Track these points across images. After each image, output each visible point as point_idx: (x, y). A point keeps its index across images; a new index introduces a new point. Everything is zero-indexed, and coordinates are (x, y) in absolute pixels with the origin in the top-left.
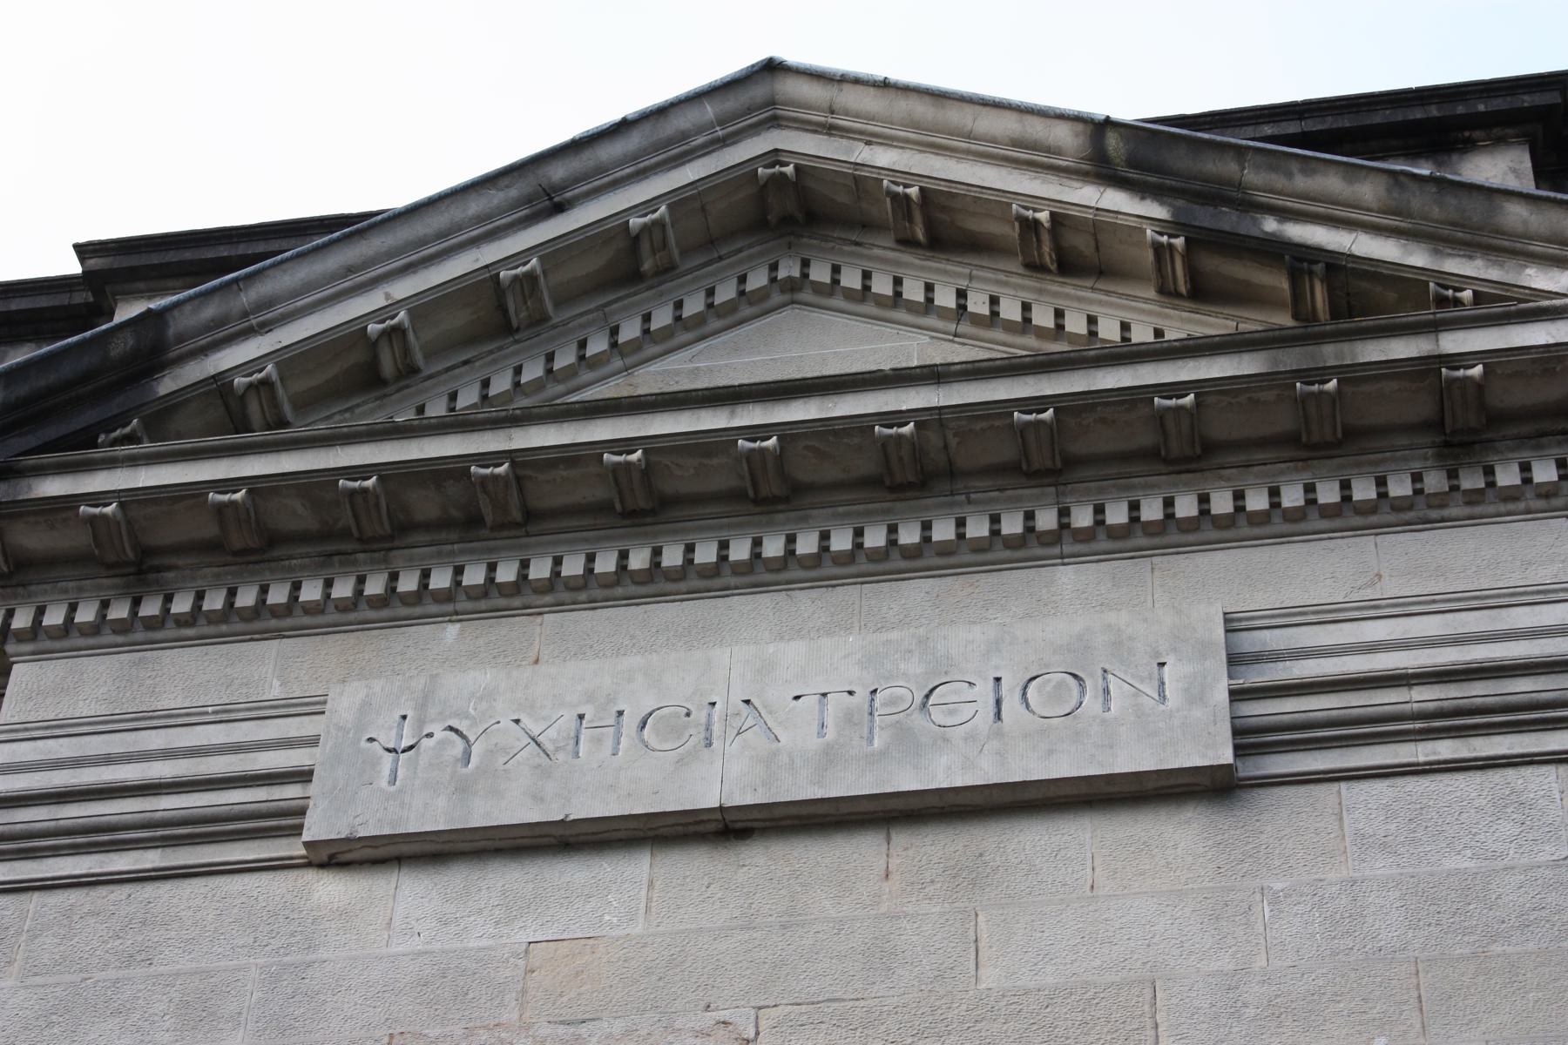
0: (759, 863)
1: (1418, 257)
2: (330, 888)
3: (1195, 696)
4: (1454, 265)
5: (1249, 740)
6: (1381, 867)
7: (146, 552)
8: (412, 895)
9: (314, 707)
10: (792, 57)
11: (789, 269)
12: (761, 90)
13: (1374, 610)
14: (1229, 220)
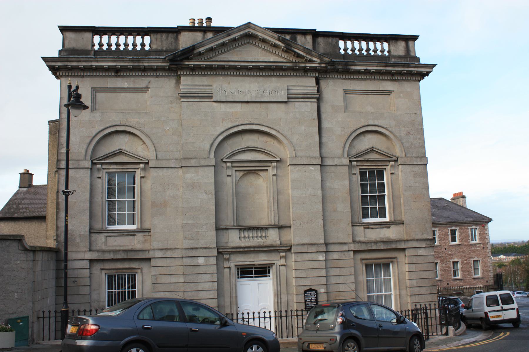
0: (250, 105)
1: (305, 55)
2: (215, 104)
3: (285, 94)
4: (308, 56)
5: (288, 98)
6: (297, 110)
7: (308, 308)
8: (222, 105)
9: (211, 86)
10: (252, 22)
11: (248, 41)
12: (248, 25)
13: (298, 86)
14: (289, 47)
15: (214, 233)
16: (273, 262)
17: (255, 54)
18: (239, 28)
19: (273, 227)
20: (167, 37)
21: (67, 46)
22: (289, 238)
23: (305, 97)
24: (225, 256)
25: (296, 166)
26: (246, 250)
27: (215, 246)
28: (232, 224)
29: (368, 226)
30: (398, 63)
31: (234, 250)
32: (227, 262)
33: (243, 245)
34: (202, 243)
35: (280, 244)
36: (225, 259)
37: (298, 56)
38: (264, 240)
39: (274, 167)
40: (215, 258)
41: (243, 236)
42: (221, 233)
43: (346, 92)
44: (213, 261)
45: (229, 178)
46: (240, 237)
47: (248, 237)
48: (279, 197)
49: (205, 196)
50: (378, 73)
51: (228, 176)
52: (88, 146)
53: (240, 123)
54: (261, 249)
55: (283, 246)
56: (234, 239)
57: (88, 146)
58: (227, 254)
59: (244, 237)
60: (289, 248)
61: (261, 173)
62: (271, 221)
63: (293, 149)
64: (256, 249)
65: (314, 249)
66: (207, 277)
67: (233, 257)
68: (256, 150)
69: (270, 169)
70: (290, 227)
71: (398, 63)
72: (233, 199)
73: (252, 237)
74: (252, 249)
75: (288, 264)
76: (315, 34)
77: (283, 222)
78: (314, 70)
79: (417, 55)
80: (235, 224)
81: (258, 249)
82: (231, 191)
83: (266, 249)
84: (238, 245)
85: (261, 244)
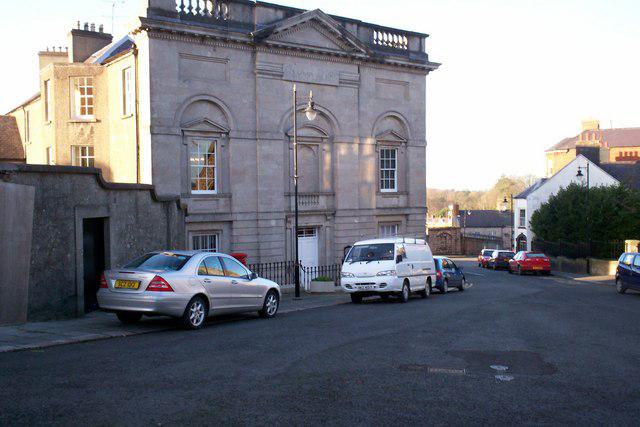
5: (340, 82)
12: (318, 11)
17: (315, 39)
18: (310, 13)
20: (243, 11)
21: (153, 5)
23: (351, 82)
29: (384, 194)
30: (407, 57)
34: (274, 207)
37: (350, 45)
43: (377, 79)
44: (282, 223)
50: (403, 66)
65: (352, 213)
66: (277, 237)
71: (407, 57)
76: (359, 24)
78: (360, 59)
79: (427, 52)
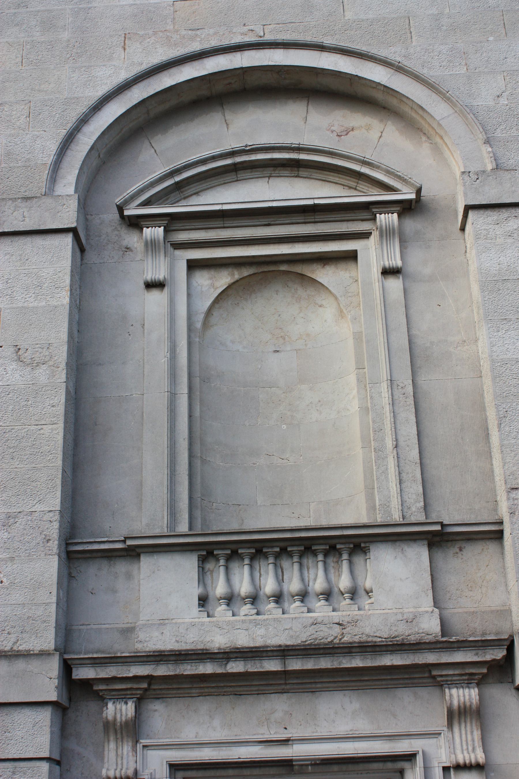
15: (50, 567)
16: (402, 747)
19: (396, 536)
22: (493, 600)
24: (111, 710)
25: (505, 213)
26: (236, 667)
27: (47, 640)
28: (161, 526)
31: (162, 670)
32: (126, 748)
33: (219, 641)
35: (444, 632)
36: (109, 727)
38: (346, 610)
39: (386, 234)
40: (45, 716)
41: (220, 588)
42: (96, 577)
45: (155, 295)
46: (203, 601)
47: (254, 599)
48: (421, 379)
49: (15, 375)
51: (150, 285)
52: (117, 752)
53: (214, 43)
54: (325, 663)
55: (463, 645)
56: (166, 607)
57: (117, 752)
58: (122, 696)
59: (230, 599)
60: (500, 654)
61: (325, 275)
62: (386, 506)
63: (481, 137)
64: (296, 665)
67: (161, 717)
68: (294, 166)
69: (373, 254)
70: (498, 536)
72: (173, 397)
73: (278, 598)
74: (272, 665)
75: (499, 757)
77: (452, 513)
80: (183, 527)
81: (309, 665)
82: (163, 361)
83: (357, 662)
84: (190, 641)
85: (328, 634)
